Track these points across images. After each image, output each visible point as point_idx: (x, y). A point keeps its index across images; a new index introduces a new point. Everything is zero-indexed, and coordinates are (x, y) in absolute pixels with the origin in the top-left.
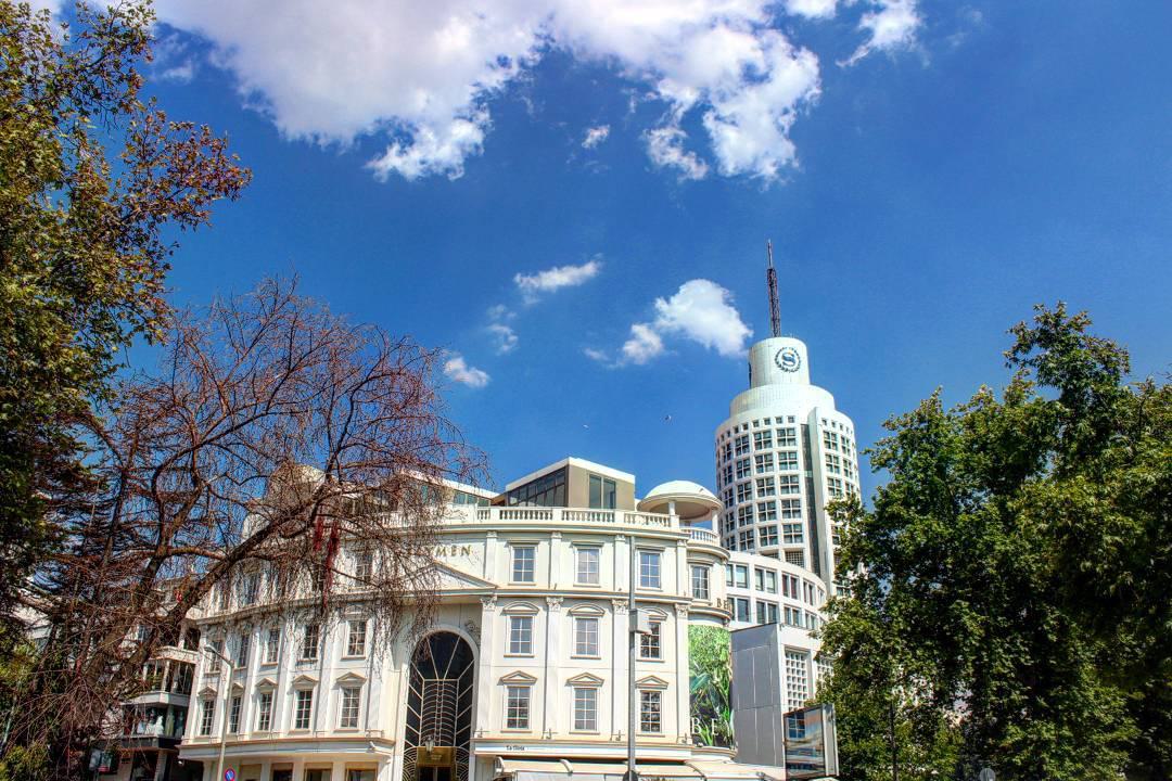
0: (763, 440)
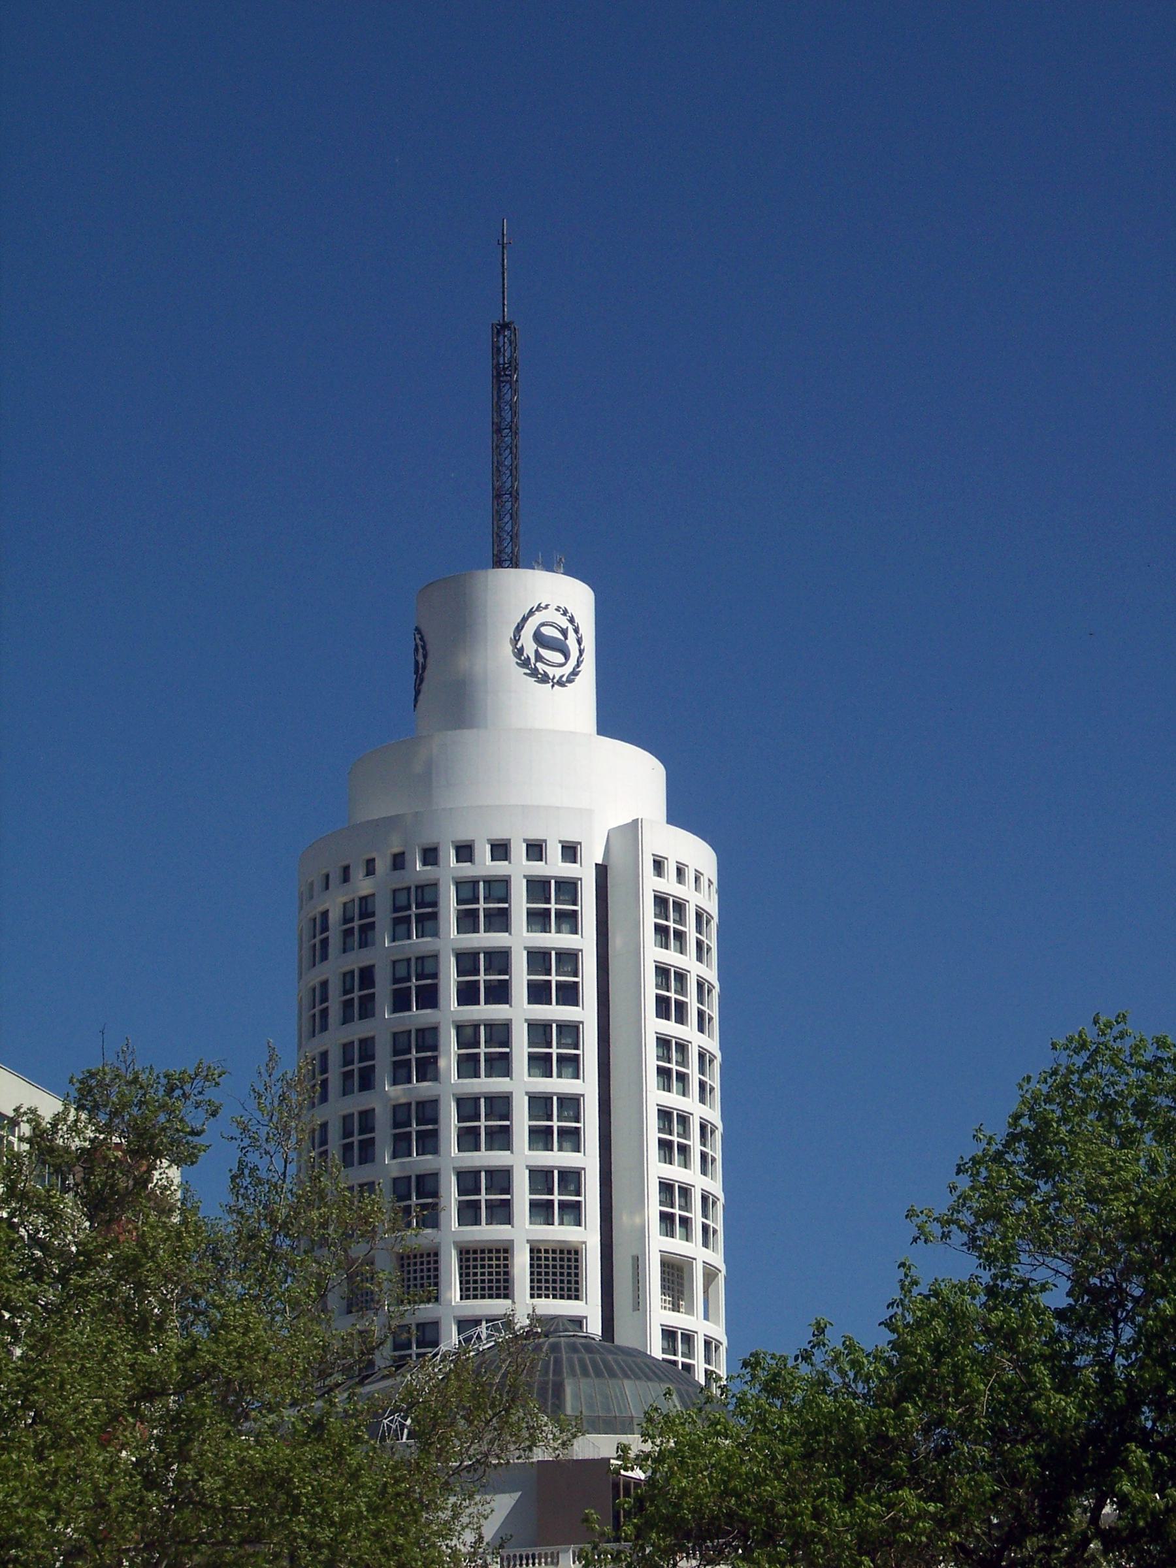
0: (486, 903)
